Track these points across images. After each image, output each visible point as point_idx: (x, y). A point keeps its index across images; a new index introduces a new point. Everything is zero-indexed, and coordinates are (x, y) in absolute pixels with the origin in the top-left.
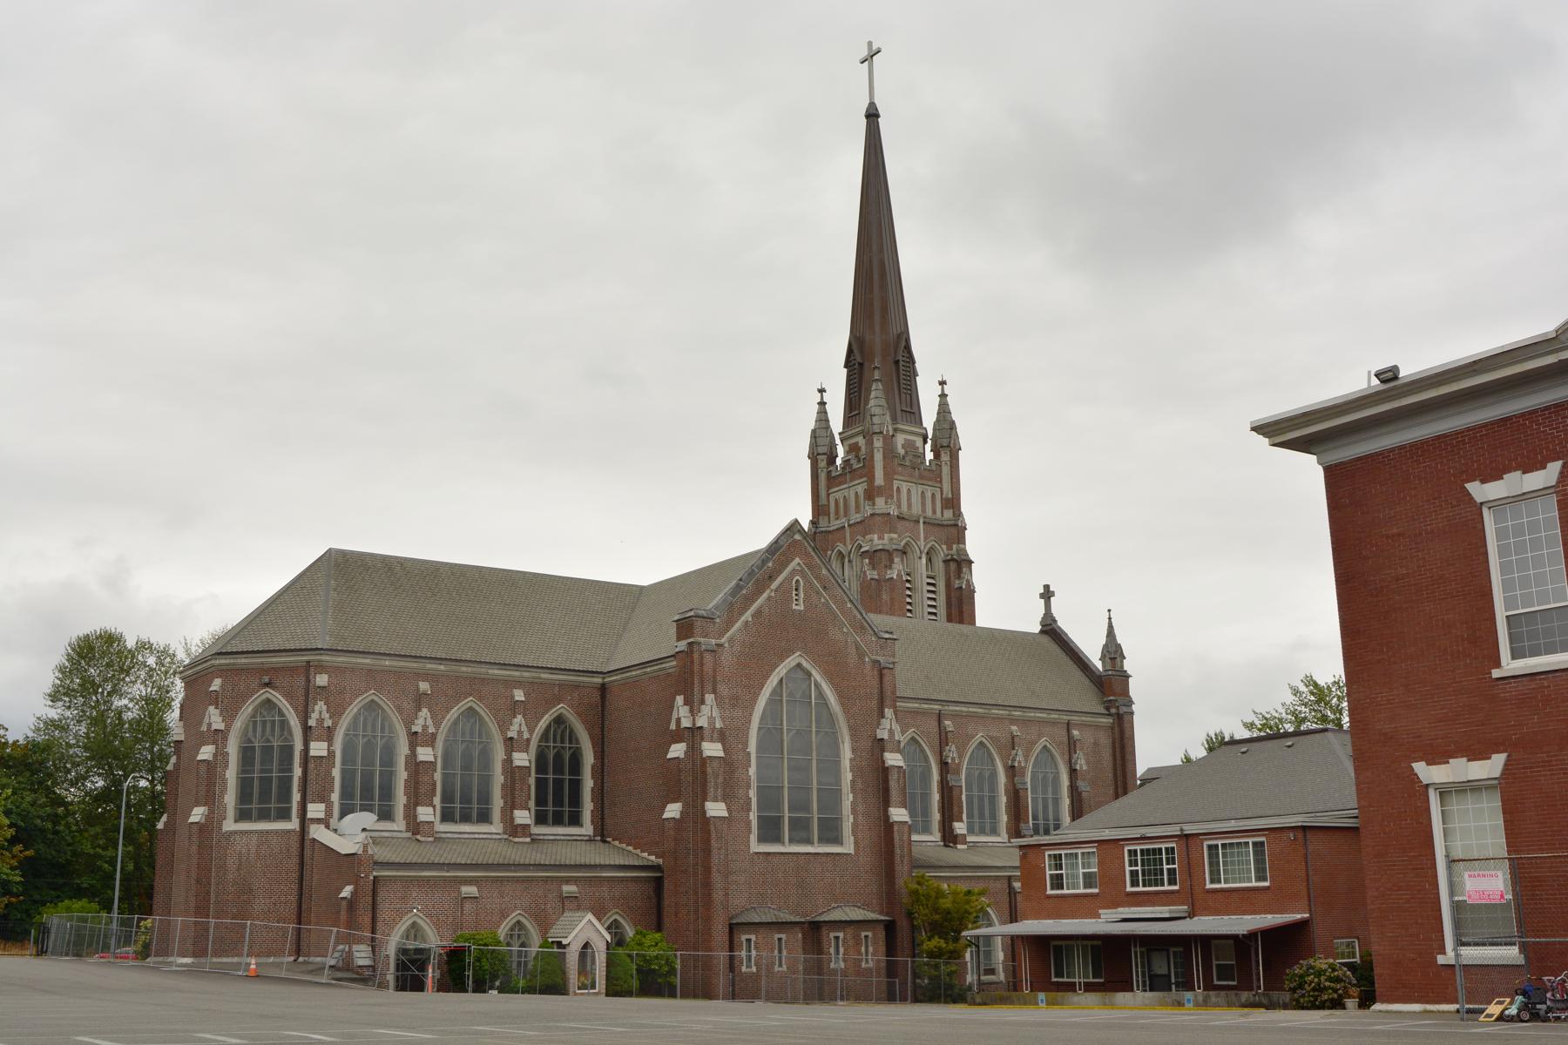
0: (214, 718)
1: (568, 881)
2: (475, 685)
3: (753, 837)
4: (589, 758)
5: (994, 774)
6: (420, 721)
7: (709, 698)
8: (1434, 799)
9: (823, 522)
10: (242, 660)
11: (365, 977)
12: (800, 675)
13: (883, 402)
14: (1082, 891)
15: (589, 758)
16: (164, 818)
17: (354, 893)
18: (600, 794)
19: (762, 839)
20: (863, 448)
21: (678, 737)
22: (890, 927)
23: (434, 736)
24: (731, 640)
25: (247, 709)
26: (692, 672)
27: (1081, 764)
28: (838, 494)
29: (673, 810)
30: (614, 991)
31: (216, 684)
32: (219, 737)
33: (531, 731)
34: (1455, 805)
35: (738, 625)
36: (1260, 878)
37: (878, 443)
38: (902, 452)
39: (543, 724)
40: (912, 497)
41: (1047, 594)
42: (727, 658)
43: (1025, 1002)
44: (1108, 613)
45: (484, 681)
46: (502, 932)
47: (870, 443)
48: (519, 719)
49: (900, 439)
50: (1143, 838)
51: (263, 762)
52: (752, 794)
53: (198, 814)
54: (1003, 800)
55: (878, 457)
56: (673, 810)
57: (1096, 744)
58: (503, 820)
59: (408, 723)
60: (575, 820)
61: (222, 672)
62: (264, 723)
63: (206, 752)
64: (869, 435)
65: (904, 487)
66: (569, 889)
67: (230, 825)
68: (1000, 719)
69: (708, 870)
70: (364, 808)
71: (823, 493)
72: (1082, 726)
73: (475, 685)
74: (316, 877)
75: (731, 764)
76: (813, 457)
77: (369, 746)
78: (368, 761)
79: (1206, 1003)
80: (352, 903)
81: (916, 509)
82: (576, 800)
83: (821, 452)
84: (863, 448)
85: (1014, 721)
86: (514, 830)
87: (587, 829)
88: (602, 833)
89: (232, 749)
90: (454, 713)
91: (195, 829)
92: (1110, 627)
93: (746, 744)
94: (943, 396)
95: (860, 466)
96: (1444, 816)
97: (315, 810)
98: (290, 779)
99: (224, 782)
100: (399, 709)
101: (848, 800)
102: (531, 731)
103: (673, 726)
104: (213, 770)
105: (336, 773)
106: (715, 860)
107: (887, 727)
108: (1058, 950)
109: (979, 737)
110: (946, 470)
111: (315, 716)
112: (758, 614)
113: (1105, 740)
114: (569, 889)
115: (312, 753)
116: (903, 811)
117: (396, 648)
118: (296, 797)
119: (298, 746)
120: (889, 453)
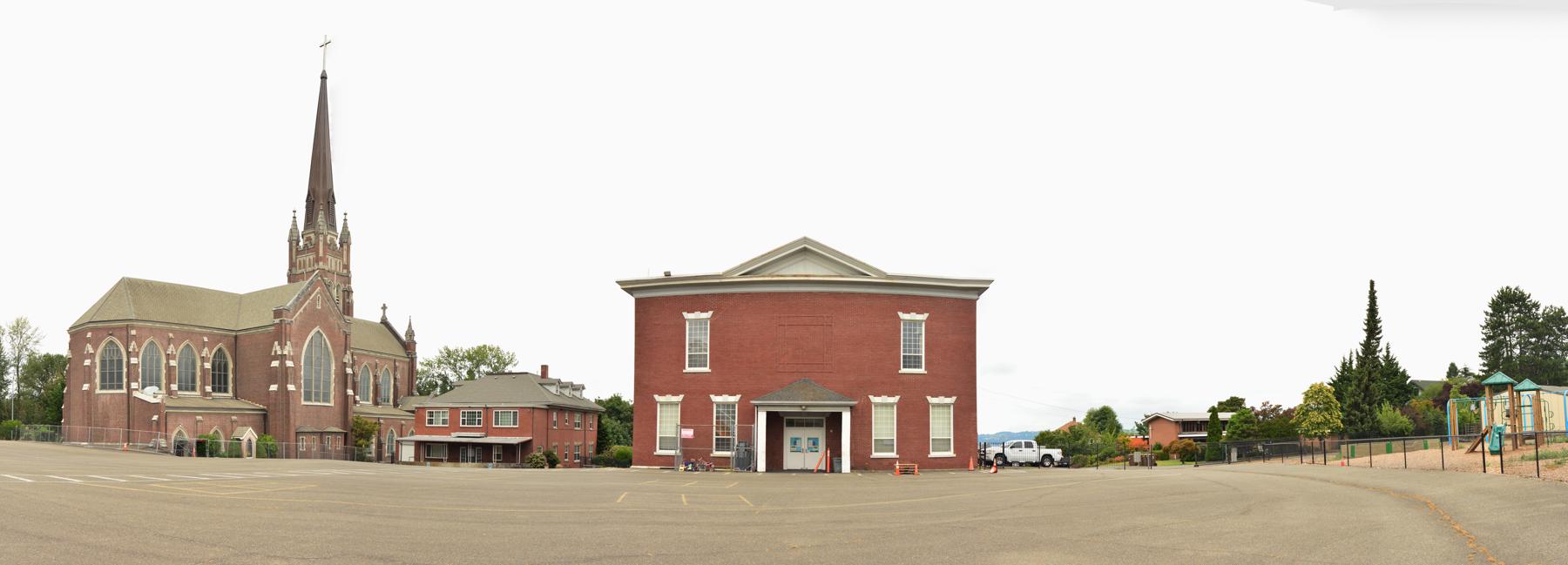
0: (90, 349)
1: (234, 414)
2: (189, 335)
3: (302, 399)
4: (231, 366)
5: (369, 378)
6: (170, 350)
7: (288, 343)
8: (658, 405)
9: (294, 271)
10: (100, 325)
11: (164, 451)
12: (318, 335)
13: (324, 220)
14: (441, 425)
15: (231, 366)
16: (66, 388)
17: (159, 418)
18: (235, 380)
19: (305, 400)
20: (313, 239)
21: (276, 358)
22: (346, 434)
23: (138, 353)
24: (295, 320)
25: (103, 344)
26: (281, 332)
27: (398, 376)
28: (301, 258)
29: (274, 388)
30: (259, 456)
31: (89, 335)
32: (92, 356)
33: (210, 354)
34: (664, 408)
35: (298, 313)
36: (515, 423)
37: (321, 238)
38: (329, 242)
39: (214, 351)
40: (332, 263)
41: (384, 308)
42: (294, 327)
43: (422, 465)
44: (382, 311)
45: (193, 333)
46: (211, 433)
47: (317, 238)
48: (206, 349)
49: (329, 237)
50: (470, 408)
51: (110, 366)
52: (302, 382)
53: (86, 387)
54: (372, 388)
55: (321, 244)
56: (274, 388)
57: (403, 368)
58: (166, 388)
59: (165, 350)
60: (226, 391)
61: (92, 330)
62: (110, 350)
63: (87, 362)
64: (317, 234)
65: (330, 258)
66: (234, 418)
67: (98, 391)
68: (372, 356)
69: (288, 411)
70: (151, 385)
71: (294, 258)
72: (400, 361)
73: (189, 335)
74: (136, 412)
75: (296, 370)
76: (290, 241)
77: (151, 359)
78: (151, 366)
79: (497, 467)
80: (158, 422)
81: (333, 269)
82: (226, 383)
83: (293, 240)
84: (313, 239)
85: (377, 358)
86: (205, 394)
87: (230, 394)
88: (236, 396)
89: (97, 360)
90: (182, 346)
91: (85, 393)
92: (410, 323)
93: (300, 362)
94: (345, 220)
95: (311, 247)
96: (661, 411)
97: (134, 385)
98: (122, 373)
99: (95, 374)
100: (162, 344)
101: (333, 385)
102: (210, 354)
103: (273, 354)
104: (91, 369)
105: (140, 370)
106: (291, 408)
107: (347, 359)
108: (429, 447)
109: (365, 363)
110: (345, 252)
111: (131, 347)
112: (305, 309)
113: (406, 367)
114: (234, 418)
115: (132, 362)
116: (293, 386)
117: (160, 319)
118: (125, 380)
119: (125, 360)
120: (325, 242)
